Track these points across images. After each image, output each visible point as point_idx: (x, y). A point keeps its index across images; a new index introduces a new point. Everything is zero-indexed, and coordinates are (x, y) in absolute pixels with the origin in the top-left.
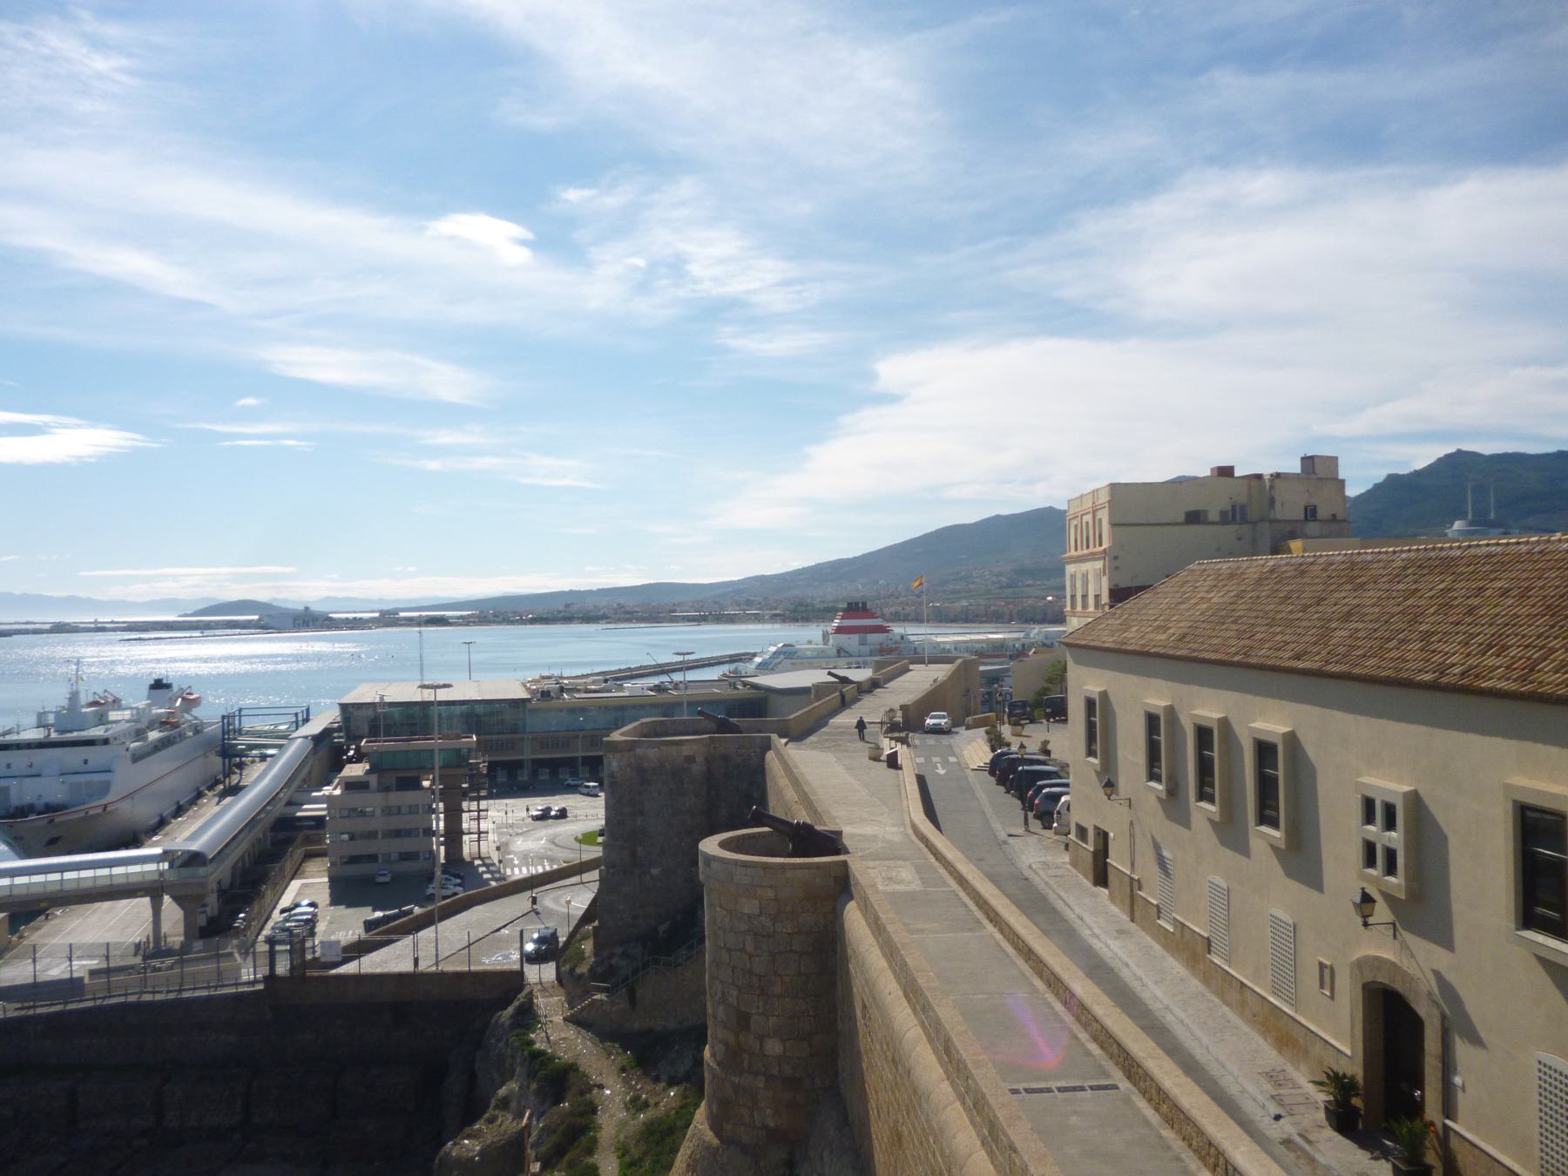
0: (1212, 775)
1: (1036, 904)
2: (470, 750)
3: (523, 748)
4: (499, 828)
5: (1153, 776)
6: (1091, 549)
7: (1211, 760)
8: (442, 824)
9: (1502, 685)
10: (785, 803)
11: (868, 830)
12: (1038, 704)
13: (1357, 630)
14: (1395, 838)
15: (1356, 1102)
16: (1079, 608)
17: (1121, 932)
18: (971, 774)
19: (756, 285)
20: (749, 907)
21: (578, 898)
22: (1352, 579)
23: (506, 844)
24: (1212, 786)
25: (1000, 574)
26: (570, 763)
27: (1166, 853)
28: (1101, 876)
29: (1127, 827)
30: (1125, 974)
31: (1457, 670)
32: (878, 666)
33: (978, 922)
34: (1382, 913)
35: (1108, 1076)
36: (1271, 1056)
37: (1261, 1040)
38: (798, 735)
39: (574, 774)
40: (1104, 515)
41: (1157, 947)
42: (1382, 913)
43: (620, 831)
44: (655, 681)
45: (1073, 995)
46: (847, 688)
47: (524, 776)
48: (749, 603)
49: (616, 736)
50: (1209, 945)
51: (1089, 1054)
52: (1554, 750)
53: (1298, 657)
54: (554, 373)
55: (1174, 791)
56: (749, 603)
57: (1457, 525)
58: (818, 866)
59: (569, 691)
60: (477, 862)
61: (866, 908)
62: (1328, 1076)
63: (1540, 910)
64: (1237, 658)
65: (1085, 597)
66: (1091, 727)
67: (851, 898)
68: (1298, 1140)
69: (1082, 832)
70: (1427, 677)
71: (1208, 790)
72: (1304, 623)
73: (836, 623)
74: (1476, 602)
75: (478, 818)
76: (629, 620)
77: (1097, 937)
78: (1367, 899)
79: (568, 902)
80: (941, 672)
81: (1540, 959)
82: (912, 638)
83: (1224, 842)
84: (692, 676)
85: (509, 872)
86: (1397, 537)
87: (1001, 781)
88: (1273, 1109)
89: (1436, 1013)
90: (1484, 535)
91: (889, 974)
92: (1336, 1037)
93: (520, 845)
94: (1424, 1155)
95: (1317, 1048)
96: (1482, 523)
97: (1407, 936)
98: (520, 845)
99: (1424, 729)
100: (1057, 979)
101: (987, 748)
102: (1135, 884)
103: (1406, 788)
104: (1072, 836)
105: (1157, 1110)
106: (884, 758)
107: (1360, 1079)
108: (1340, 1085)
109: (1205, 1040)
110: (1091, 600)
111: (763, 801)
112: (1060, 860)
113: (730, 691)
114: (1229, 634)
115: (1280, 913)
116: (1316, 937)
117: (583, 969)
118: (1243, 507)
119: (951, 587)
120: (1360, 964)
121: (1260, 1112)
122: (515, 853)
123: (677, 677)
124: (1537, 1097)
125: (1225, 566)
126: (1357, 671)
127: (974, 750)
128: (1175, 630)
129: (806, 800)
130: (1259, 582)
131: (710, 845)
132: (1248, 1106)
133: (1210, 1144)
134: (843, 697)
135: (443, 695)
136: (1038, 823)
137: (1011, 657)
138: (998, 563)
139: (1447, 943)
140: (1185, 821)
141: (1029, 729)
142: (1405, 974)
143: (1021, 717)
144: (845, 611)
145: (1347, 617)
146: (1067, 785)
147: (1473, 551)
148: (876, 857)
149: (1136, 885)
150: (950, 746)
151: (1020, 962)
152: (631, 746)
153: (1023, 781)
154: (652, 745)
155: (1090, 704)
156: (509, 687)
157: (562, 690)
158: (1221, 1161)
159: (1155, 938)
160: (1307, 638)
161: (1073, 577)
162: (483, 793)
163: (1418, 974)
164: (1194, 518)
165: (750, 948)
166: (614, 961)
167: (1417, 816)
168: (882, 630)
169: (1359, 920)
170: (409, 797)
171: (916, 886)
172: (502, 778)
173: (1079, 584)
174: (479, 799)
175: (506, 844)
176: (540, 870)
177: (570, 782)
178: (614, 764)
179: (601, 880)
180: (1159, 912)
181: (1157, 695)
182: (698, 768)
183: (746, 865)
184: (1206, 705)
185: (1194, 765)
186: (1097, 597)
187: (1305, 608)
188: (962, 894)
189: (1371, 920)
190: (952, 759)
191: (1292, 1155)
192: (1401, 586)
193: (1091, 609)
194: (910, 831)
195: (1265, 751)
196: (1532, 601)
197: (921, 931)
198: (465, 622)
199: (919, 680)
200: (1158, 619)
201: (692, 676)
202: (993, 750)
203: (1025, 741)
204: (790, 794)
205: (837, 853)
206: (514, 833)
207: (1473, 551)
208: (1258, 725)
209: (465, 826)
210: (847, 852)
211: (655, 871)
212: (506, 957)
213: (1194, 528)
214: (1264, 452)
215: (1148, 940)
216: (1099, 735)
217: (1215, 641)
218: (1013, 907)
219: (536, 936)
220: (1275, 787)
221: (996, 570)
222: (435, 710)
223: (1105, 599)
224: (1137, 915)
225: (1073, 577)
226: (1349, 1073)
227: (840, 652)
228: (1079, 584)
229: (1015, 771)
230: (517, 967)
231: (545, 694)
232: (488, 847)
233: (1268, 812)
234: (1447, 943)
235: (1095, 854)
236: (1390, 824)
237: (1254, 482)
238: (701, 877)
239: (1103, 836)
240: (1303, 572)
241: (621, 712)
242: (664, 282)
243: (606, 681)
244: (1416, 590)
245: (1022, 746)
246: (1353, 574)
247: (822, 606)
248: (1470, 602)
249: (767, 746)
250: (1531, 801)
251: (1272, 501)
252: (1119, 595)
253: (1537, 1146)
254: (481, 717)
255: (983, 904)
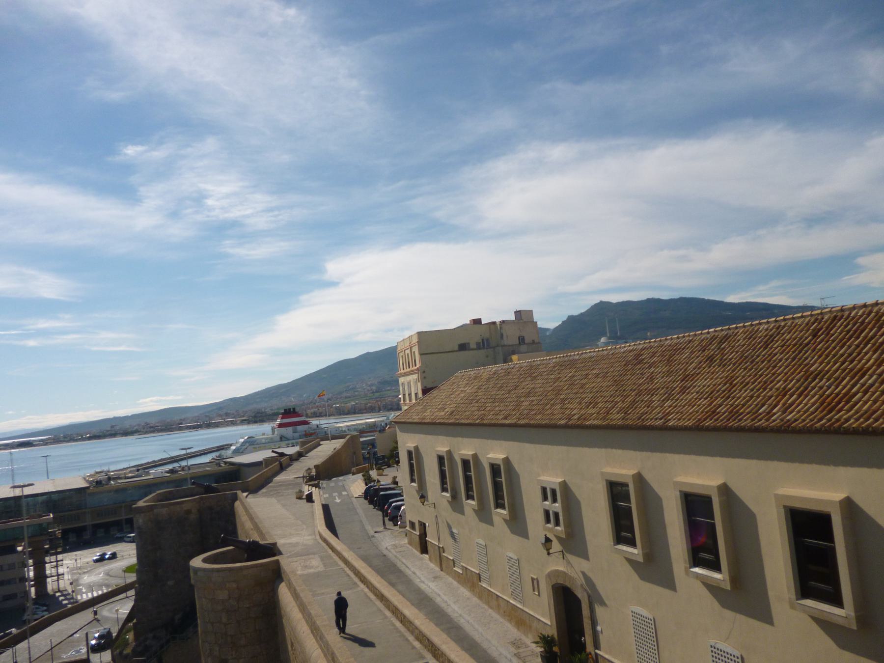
1: (389, 570)
2: (49, 524)
3: (82, 518)
4: (71, 571)
5: (444, 489)
6: (411, 368)
7: (471, 477)
8: (32, 574)
9: (596, 422)
10: (247, 533)
11: (294, 540)
13: (533, 401)
14: (557, 507)
17: (435, 578)
18: (354, 500)
19: (249, 212)
20: (222, 595)
21: (124, 607)
23: (77, 580)
25: (372, 385)
26: (118, 524)
27: (454, 531)
28: (424, 548)
30: (438, 600)
31: (576, 417)
32: (303, 444)
33: (355, 583)
34: (556, 546)
36: (514, 632)
37: (509, 625)
38: (254, 489)
39: (121, 530)
40: (416, 349)
41: (455, 583)
42: (556, 546)
43: (147, 564)
44: (170, 467)
45: (405, 617)
46: (283, 459)
47: (87, 536)
48: (227, 415)
49: (141, 504)
51: (414, 648)
52: (620, 452)
53: (505, 418)
54: (108, 276)
55: (455, 497)
56: (227, 415)
57: (603, 340)
58: (262, 565)
59: (115, 479)
60: (58, 594)
61: (290, 587)
62: (541, 638)
63: (623, 534)
65: (410, 395)
66: (411, 466)
67: (282, 581)
69: (412, 525)
70: (563, 422)
73: (278, 421)
74: (584, 381)
75: (57, 566)
76: (153, 432)
77: (423, 582)
78: (548, 540)
79: (117, 611)
80: (338, 444)
82: (323, 426)
84: (192, 462)
85: (79, 597)
87: (371, 502)
89: (585, 594)
90: (617, 344)
91: (303, 622)
92: (543, 615)
93: (86, 579)
96: (615, 338)
97: (569, 556)
98: (86, 579)
99: (564, 448)
101: (363, 485)
102: (441, 550)
103: (560, 480)
104: (408, 528)
106: (304, 497)
107: (556, 636)
109: (480, 630)
111: (234, 532)
113: (217, 468)
114: (474, 409)
115: (511, 555)
116: (519, 561)
117: (128, 651)
118: (487, 340)
119: (345, 394)
120: (549, 576)
122: (83, 585)
123: (184, 463)
124: (633, 630)
125: (473, 373)
126: (532, 422)
127: (356, 486)
129: (257, 527)
130: (488, 380)
131: (197, 562)
134: (281, 464)
135: (28, 491)
138: (361, 380)
139: (587, 558)
142: (570, 577)
144: (283, 414)
145: (528, 394)
146: (403, 500)
147: (584, 356)
148: (298, 555)
150: (343, 486)
151: (378, 603)
152: (150, 508)
153: (381, 500)
154: (163, 506)
155: (410, 453)
156: (74, 481)
157: (110, 479)
159: (454, 578)
161: (403, 384)
162: (59, 550)
163: (576, 576)
164: (463, 347)
165: (224, 620)
166: (148, 643)
167: (564, 494)
168: (305, 423)
169: (546, 552)
170: (9, 559)
171: (321, 568)
172: (72, 538)
174: (57, 554)
175: (77, 580)
176: (100, 593)
177: (118, 535)
178: (141, 521)
179: (136, 595)
181: (440, 445)
182: (193, 517)
183: (218, 570)
184: (466, 448)
186: (416, 394)
187: (510, 391)
188: (347, 569)
189: (551, 551)
190: (344, 493)
192: (552, 376)
193: (414, 401)
194: (318, 537)
196: (609, 378)
197: (323, 594)
198: (45, 443)
199: (326, 449)
201: (192, 462)
202: (366, 484)
204: (248, 525)
205: (274, 555)
206: (82, 572)
207: (584, 356)
208: (491, 455)
209: (48, 572)
210: (280, 553)
211: (171, 583)
212: (78, 652)
213: (462, 353)
214: (496, 310)
215: (450, 579)
216: (416, 471)
217: (467, 413)
218: (373, 572)
219: (97, 635)
220: (496, 490)
222: (24, 502)
223: (420, 395)
224: (444, 567)
225: (403, 384)
227: (282, 438)
230: (85, 657)
231: (99, 483)
232: (64, 584)
233: (500, 501)
234: (587, 558)
235: (420, 536)
237: (492, 326)
238: (193, 582)
239: (423, 526)
241: (148, 487)
242: (190, 211)
243: (138, 470)
247: (271, 412)
249: (235, 498)
250: (614, 479)
251: (502, 336)
252: (425, 391)
254: (57, 502)
255: (357, 573)
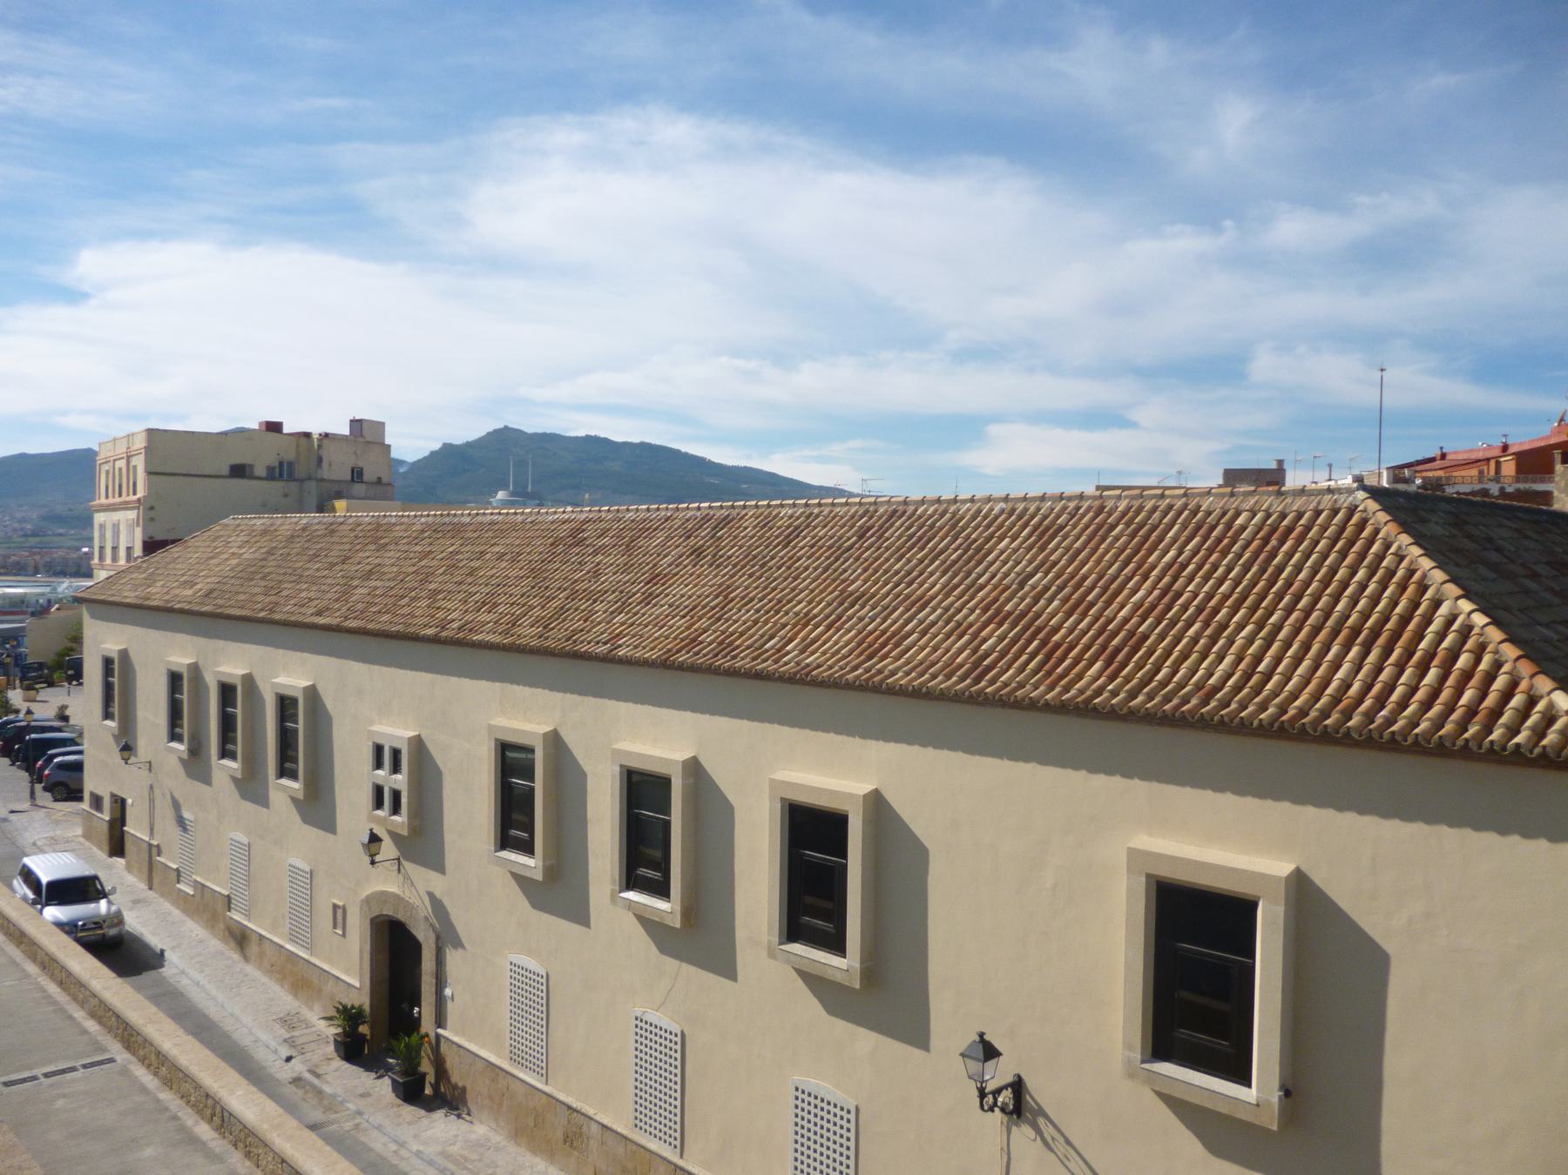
0: (234, 730)
5: (174, 736)
6: (124, 498)
9: (491, 638)
12: (59, 665)
14: (400, 780)
15: (364, 1029)
16: (108, 561)
22: (376, 540)
24: (295, 761)
25: (24, 520)
27: (186, 815)
29: (146, 793)
34: (388, 849)
35: (103, 1050)
36: (286, 1001)
37: (277, 988)
40: (139, 462)
41: (176, 912)
42: (388, 849)
45: (69, 974)
50: (229, 902)
51: (85, 1032)
53: (319, 613)
55: (197, 750)
57: (501, 495)
62: (338, 1011)
63: (514, 832)
64: (261, 615)
65: (115, 549)
66: (108, 688)
68: (308, 1076)
69: (97, 802)
70: (430, 632)
71: (230, 747)
72: (329, 581)
78: (374, 839)
81: (514, 875)
83: (307, 819)
86: (449, 503)
88: (285, 1052)
90: (525, 505)
92: (347, 971)
94: (419, 1064)
95: (329, 986)
96: (523, 495)
100: (53, 960)
102: (154, 850)
103: (412, 734)
105: (156, 1074)
108: (350, 1017)
110: (122, 553)
112: (70, 834)
114: (256, 590)
118: (290, 464)
120: (368, 901)
121: (272, 1057)
126: (371, 626)
128: (202, 586)
130: (291, 539)
132: (261, 1055)
133: (207, 1096)
136: (48, 795)
137: (33, 614)
139: (441, 869)
140: (206, 779)
141: (46, 694)
143: (37, 680)
145: (368, 575)
146: (80, 752)
147: (480, 518)
149: (154, 851)
158: (218, 1110)
159: (175, 903)
160: (329, 595)
161: (102, 526)
163: (418, 902)
164: (239, 471)
169: (368, 860)
173: (109, 534)
180: (179, 875)
184: (230, 661)
185: (216, 723)
186: (129, 549)
187: (332, 565)
189: (377, 858)
191: (300, 1092)
192: (418, 548)
195: (286, 705)
200: (196, 569)
203: (34, 707)
207: (480, 518)
214: (317, 413)
215: (167, 906)
217: (242, 597)
221: (19, 515)
224: (156, 881)
225: (102, 526)
226: (357, 1004)
228: (109, 534)
229: (21, 740)
234: (441, 869)
235: (112, 823)
236: (396, 768)
237: (303, 441)
240: (333, 531)
244: (430, 552)
245: (29, 712)
246: (377, 536)
248: (472, 564)
251: (320, 460)
252: (151, 546)
253: (508, 1035)
